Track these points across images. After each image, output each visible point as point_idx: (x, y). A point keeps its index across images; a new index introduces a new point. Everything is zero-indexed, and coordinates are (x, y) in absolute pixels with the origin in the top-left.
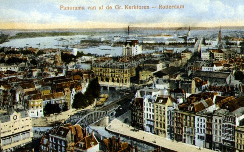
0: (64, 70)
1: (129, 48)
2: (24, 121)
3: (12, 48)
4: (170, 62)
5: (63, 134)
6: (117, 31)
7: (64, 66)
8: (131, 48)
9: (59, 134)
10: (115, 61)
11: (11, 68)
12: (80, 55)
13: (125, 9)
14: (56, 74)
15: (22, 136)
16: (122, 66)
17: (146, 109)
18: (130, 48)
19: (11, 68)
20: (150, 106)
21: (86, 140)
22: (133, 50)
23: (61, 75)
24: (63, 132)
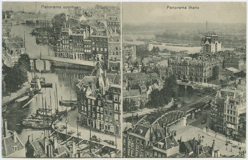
1: (208, 44)
18: (209, 44)
21: (166, 140)
22: (212, 47)
24: (142, 131)
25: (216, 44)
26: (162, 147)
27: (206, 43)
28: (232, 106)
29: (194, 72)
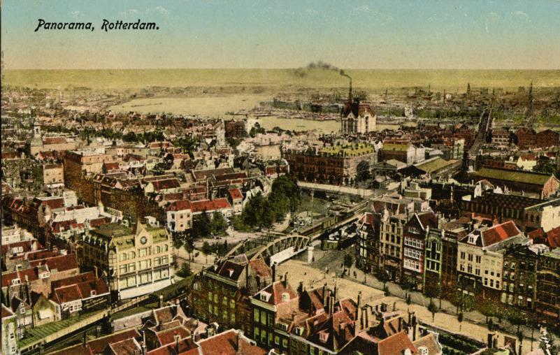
0: (231, 157)
2: (125, 242)
3: (134, 114)
4: (431, 149)
5: (233, 275)
6: (258, 85)
7: (441, 172)
8: (356, 122)
9: (225, 274)
10: (326, 144)
11: (134, 151)
12: (259, 129)
13: (102, 28)
14: (217, 164)
15: (155, 276)
16: (340, 153)
17: (384, 236)
18: (354, 119)
19: (134, 151)
20: (393, 231)
22: (359, 124)
23: (222, 166)
24: (231, 272)
25: (367, 118)
26: (267, 300)
27: (349, 116)
28: (393, 227)
29: (327, 168)
